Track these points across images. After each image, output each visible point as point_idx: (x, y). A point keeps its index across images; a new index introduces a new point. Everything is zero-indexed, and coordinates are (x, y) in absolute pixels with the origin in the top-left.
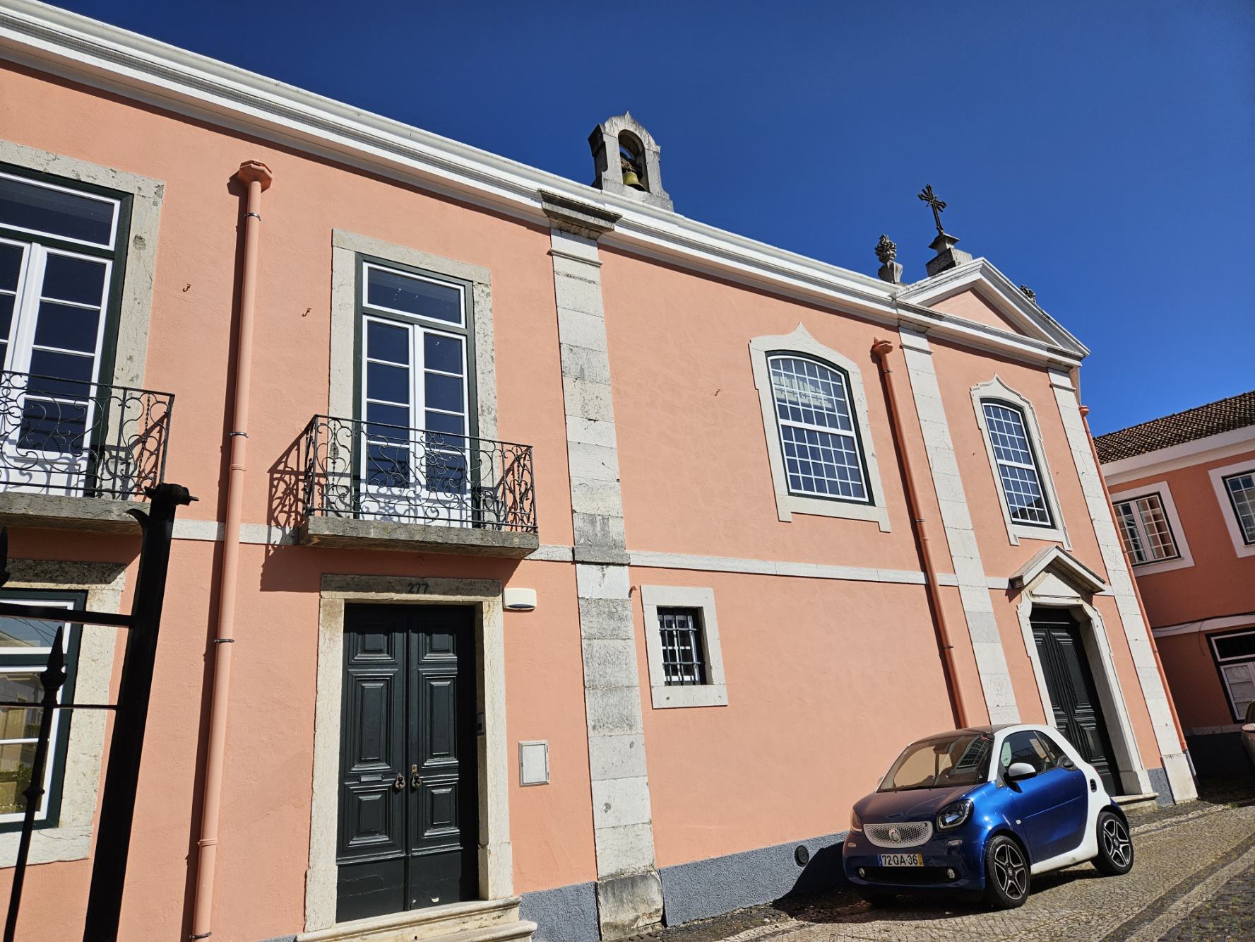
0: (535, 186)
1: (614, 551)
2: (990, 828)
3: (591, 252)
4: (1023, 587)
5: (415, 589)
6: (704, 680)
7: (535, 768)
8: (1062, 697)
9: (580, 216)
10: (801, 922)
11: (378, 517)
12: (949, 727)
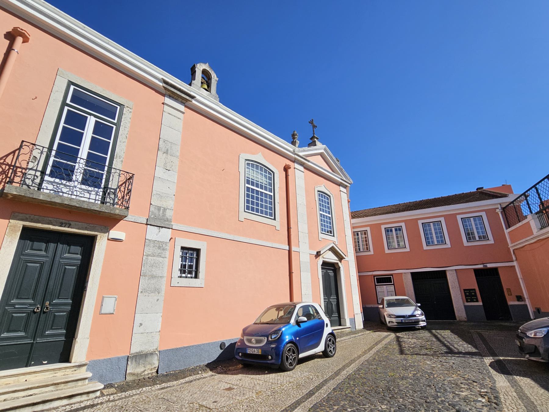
0: (161, 77)
1: (166, 223)
2: (287, 340)
3: (182, 108)
4: (320, 255)
5: (64, 225)
6: (196, 277)
7: (109, 305)
8: (327, 292)
9: (178, 93)
10: (213, 374)
11: (52, 192)
12: (287, 301)
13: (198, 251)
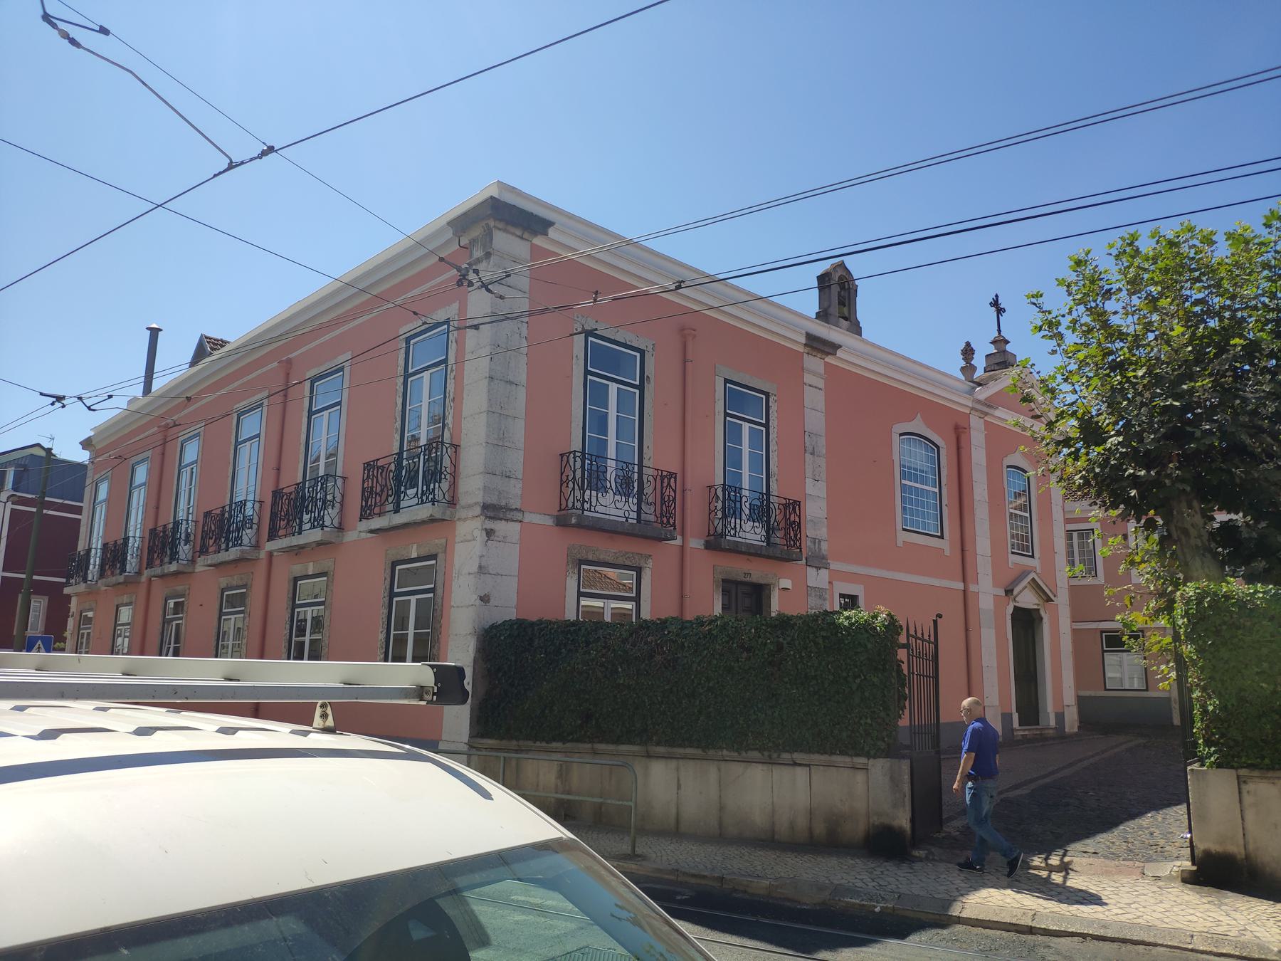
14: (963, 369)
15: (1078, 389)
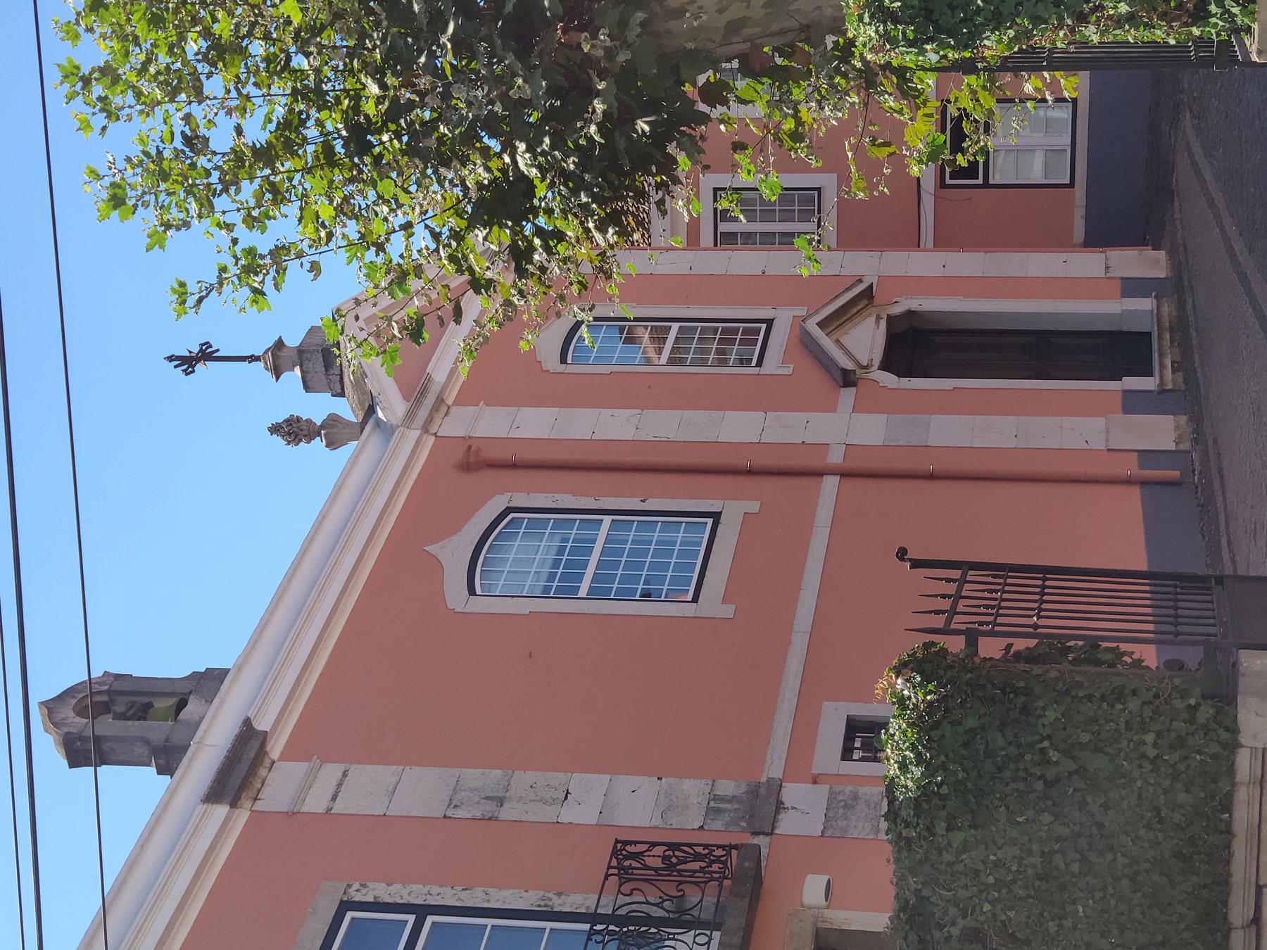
13: (716, 190)
14: (332, 444)
15: (400, 219)
